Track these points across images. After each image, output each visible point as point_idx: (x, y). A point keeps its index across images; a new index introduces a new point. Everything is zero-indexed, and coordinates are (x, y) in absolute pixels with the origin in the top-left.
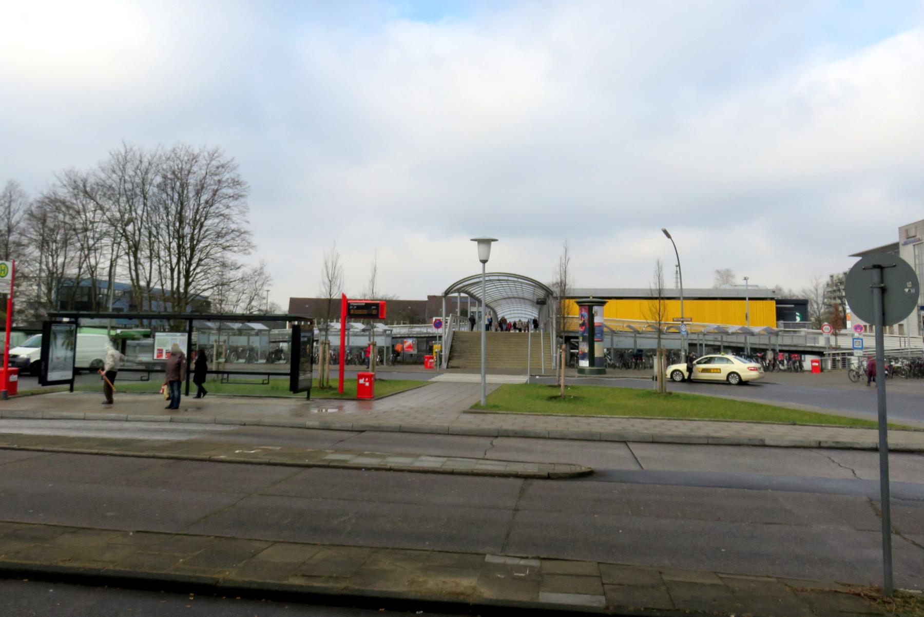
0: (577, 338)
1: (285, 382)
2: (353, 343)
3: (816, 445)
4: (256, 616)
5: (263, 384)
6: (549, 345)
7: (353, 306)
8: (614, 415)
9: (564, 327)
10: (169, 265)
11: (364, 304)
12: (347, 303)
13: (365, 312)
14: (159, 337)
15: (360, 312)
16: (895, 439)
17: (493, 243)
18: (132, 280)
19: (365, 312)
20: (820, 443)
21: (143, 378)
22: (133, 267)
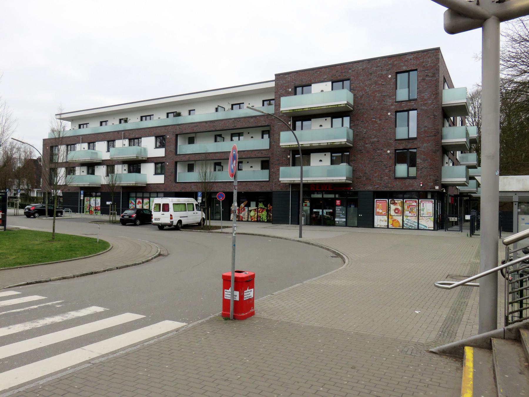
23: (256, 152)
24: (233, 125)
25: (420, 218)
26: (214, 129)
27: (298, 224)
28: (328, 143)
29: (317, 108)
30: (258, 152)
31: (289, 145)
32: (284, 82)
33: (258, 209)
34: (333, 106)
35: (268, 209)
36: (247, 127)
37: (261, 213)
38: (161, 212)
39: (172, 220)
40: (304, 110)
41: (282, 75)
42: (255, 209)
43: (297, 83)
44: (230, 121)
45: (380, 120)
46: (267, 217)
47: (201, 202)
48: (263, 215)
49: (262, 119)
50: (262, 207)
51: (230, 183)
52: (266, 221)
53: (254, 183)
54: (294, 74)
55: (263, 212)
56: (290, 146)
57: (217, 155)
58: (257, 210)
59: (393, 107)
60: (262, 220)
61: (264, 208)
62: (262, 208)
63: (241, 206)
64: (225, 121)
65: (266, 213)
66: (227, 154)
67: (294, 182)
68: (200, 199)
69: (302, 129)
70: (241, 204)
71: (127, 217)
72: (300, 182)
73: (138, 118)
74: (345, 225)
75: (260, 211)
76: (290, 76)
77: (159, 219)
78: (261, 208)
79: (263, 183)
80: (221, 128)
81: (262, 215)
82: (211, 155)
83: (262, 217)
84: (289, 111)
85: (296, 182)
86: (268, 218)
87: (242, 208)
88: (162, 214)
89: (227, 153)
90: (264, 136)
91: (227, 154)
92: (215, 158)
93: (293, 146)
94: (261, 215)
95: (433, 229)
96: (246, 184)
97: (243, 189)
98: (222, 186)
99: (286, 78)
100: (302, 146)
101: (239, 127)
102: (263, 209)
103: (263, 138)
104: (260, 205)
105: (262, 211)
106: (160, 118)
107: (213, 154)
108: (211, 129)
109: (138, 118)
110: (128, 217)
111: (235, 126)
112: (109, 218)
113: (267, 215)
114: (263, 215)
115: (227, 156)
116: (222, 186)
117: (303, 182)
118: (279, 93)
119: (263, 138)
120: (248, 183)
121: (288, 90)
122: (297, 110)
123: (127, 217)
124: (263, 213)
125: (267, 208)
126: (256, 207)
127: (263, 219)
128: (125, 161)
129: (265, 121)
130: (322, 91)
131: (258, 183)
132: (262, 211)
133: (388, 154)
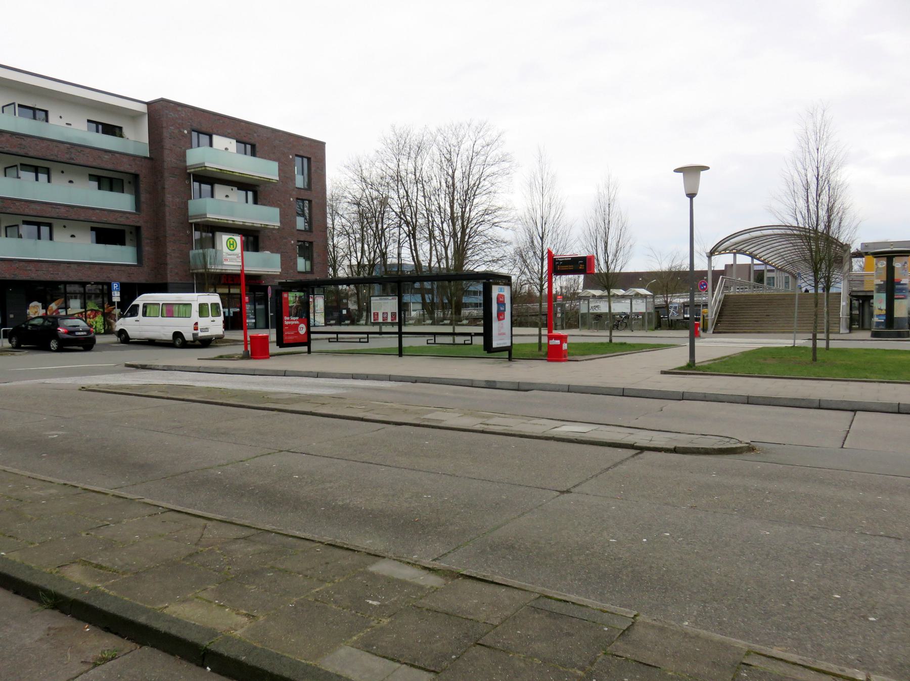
0: (872, 291)
1: (479, 341)
2: (636, 309)
3: (816, 405)
4: (1, 636)
5: (465, 344)
6: (838, 300)
7: (559, 261)
8: (615, 352)
9: (245, 147)
10: (443, 244)
11: (570, 259)
12: (553, 258)
13: (571, 267)
14: (374, 301)
15: (565, 267)
16: (404, 329)
17: (702, 173)
18: (413, 259)
19: (571, 267)
20: (748, 397)
21: (362, 340)
22: (413, 248)
23: (117, 215)
24: (68, 156)
25: (316, 314)
26: (22, 152)
27: (242, 329)
28: (261, 224)
29: (251, 177)
30: (120, 215)
31: (218, 219)
32: (177, 116)
33: (86, 312)
34: (265, 180)
35: (106, 311)
36: (98, 166)
37: (92, 320)
38: (211, 318)
39: (195, 332)
40: (234, 174)
41: (173, 105)
42: (81, 313)
43: (195, 126)
44: (62, 146)
45: (285, 204)
46: (104, 324)
47: (119, 300)
48: (96, 322)
49: (124, 160)
50: (93, 308)
51: (68, 265)
52: (103, 331)
53: (115, 268)
54: (190, 110)
55: (97, 318)
56: (220, 221)
57: (33, 206)
58: (84, 313)
59: (294, 193)
60: (96, 330)
61: (99, 310)
62: (94, 310)
63: (49, 308)
64: (49, 143)
65: (103, 318)
66: (59, 208)
67: (226, 271)
68: (116, 295)
69: (200, 197)
70: (51, 303)
71: (82, 333)
72: (240, 272)
73: (61, 117)
74: (254, 327)
75: (91, 316)
76: (185, 112)
77: (206, 329)
78: (92, 310)
79: (133, 268)
80: (40, 155)
81: (94, 323)
82: (17, 204)
83: (96, 327)
84: (215, 170)
85: (228, 271)
86: (106, 328)
87: (52, 312)
88: (138, 321)
89: (59, 207)
90: (40, 175)
91: (59, 208)
92: (27, 211)
93: (222, 221)
94: (93, 322)
95: (324, 325)
96: (102, 269)
97: (95, 277)
98: (50, 269)
99: (179, 111)
100: (234, 223)
101: (82, 163)
102: (96, 313)
103: (37, 179)
104: (91, 306)
105: (93, 316)
106: (70, 124)
107: (23, 203)
108: (14, 150)
109: (61, 117)
110: (85, 333)
111: (73, 159)
112: (613, 305)
113: (104, 322)
114: (96, 322)
115: (58, 213)
116: (50, 269)
117: (245, 272)
118: (169, 130)
119: (37, 179)
120: (105, 266)
121: (182, 130)
122: (225, 172)
123: (82, 333)
124: (97, 319)
125: (104, 310)
126: (81, 308)
127: (97, 329)
128: (222, 226)
129: (130, 165)
130: (226, 149)
131: (123, 268)
132: (95, 316)
133: (292, 245)
